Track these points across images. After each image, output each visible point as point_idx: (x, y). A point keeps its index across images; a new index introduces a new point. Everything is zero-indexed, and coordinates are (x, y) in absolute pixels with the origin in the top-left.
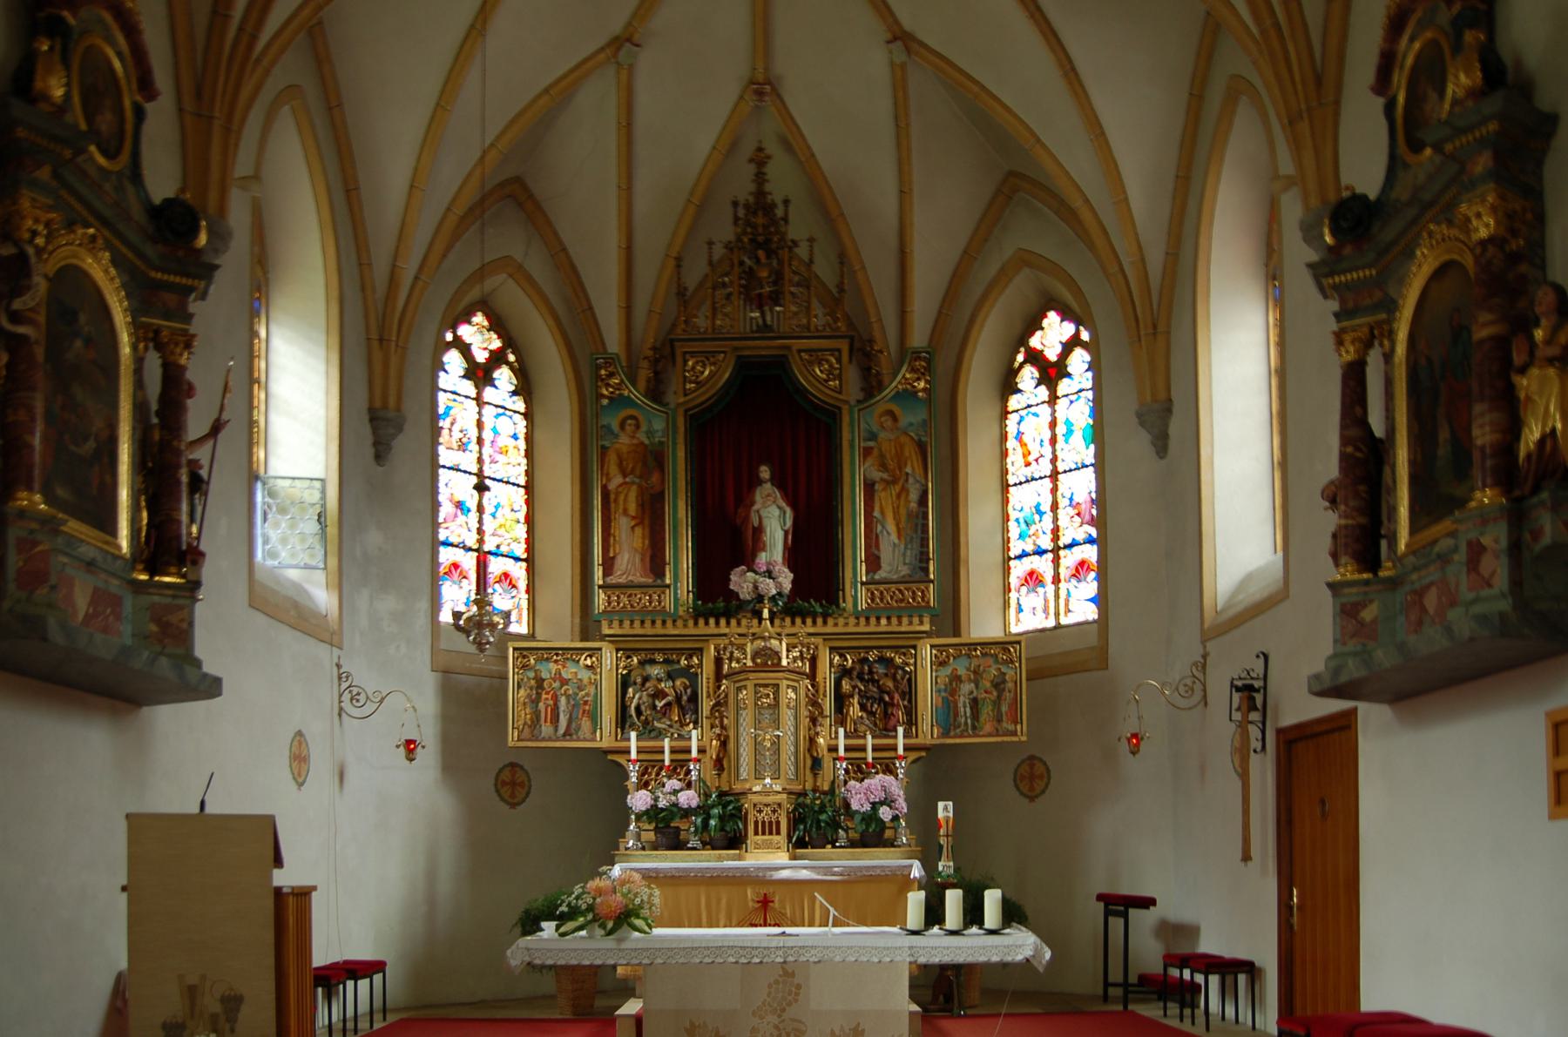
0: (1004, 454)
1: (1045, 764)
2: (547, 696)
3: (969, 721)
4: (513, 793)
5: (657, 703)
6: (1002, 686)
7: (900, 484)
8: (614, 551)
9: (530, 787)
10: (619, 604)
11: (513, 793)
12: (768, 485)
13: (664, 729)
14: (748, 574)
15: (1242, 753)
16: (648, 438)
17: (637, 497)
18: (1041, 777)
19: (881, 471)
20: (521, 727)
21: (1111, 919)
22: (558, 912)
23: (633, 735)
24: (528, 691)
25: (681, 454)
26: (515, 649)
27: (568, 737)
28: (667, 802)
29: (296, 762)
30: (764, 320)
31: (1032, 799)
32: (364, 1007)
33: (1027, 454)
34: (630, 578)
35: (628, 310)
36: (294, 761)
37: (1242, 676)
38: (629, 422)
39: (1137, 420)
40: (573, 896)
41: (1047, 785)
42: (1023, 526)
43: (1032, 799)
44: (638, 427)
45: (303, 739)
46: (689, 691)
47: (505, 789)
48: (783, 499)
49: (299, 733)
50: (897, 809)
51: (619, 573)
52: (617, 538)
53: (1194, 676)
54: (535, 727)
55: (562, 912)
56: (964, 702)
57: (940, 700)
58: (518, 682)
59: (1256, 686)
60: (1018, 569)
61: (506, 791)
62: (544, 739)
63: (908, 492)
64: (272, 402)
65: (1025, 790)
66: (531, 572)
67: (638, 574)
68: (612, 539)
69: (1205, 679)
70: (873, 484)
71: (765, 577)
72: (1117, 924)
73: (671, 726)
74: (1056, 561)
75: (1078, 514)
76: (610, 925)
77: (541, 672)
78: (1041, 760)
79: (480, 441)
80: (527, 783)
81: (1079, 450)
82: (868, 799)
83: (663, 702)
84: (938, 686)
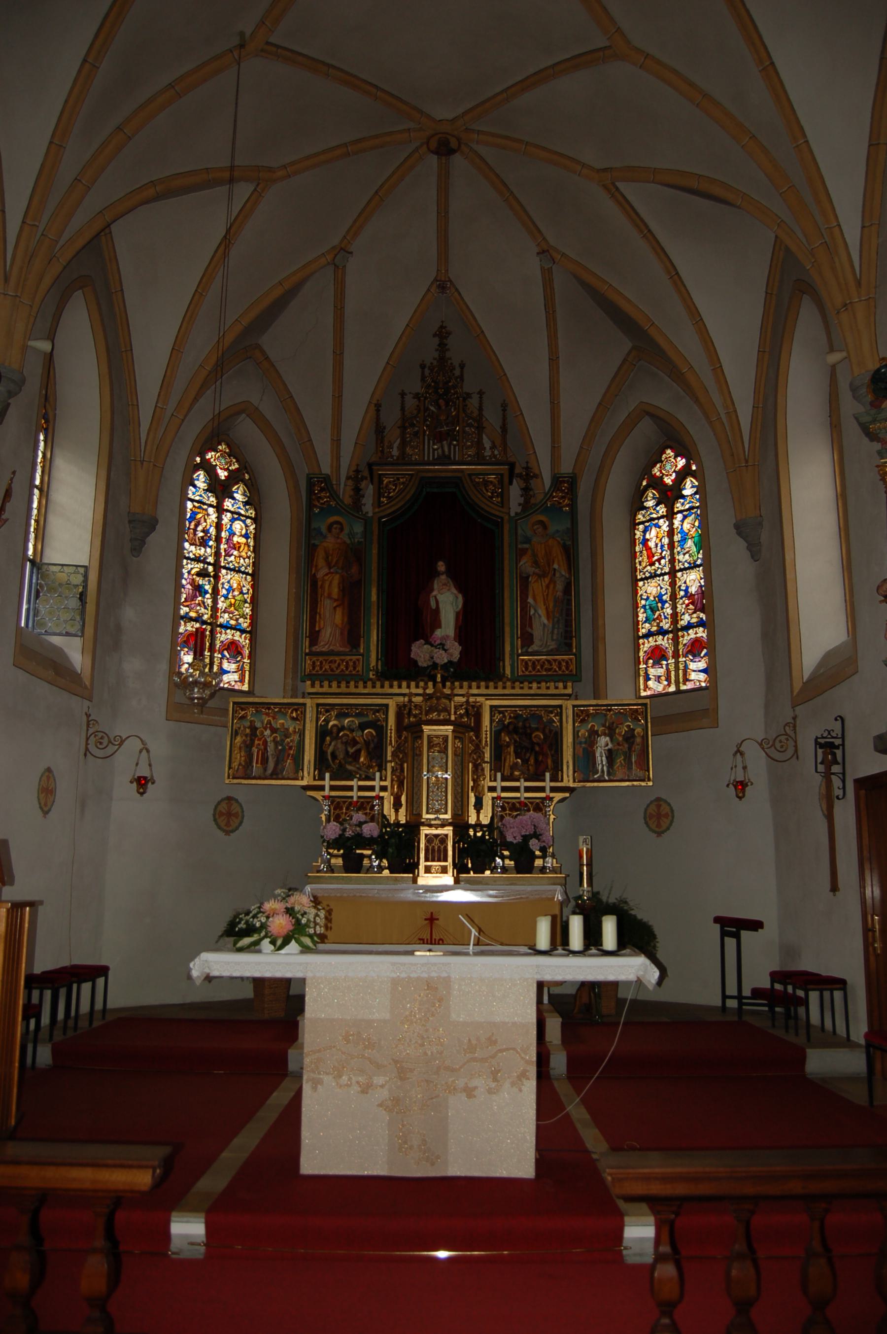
0: (634, 555)
1: (669, 804)
2: (259, 742)
3: (605, 768)
4: (228, 822)
5: (349, 749)
6: (632, 740)
7: (549, 577)
8: (319, 627)
9: (243, 817)
10: (321, 668)
11: (228, 822)
12: (443, 577)
13: (355, 772)
14: (425, 646)
15: (829, 801)
16: (350, 538)
17: (339, 584)
18: (666, 816)
19: (533, 567)
20: (237, 767)
21: (726, 939)
22: (237, 929)
23: (327, 775)
24: (244, 738)
25: (375, 551)
26: (234, 703)
27: (274, 777)
28: (353, 832)
29: (43, 795)
30: (443, 451)
31: (659, 834)
32: (85, 1007)
33: (651, 555)
34: (331, 648)
35: (337, 442)
36: (42, 793)
37: (824, 735)
38: (335, 526)
39: (735, 531)
40: (251, 915)
41: (672, 822)
42: (649, 612)
43: (659, 834)
44: (342, 530)
45: (51, 775)
46: (376, 740)
47: (222, 818)
48: (455, 587)
49: (49, 770)
50: (544, 842)
51: (322, 644)
52: (322, 616)
53: (786, 734)
54: (248, 767)
55: (241, 930)
56: (601, 752)
57: (581, 750)
58: (236, 730)
59: (836, 744)
60: (646, 645)
61: (222, 821)
62: (255, 778)
63: (555, 583)
64: (51, 507)
65: (653, 827)
66: (253, 642)
67: (338, 645)
68: (318, 617)
69: (796, 736)
70: (528, 577)
71: (439, 648)
72: (730, 942)
73: (359, 769)
74: (676, 641)
75: (692, 603)
76: (279, 942)
77: (255, 722)
78: (666, 801)
79: (218, 539)
80: (240, 814)
81: (688, 553)
82: (520, 833)
83: (354, 749)
84: (579, 739)
